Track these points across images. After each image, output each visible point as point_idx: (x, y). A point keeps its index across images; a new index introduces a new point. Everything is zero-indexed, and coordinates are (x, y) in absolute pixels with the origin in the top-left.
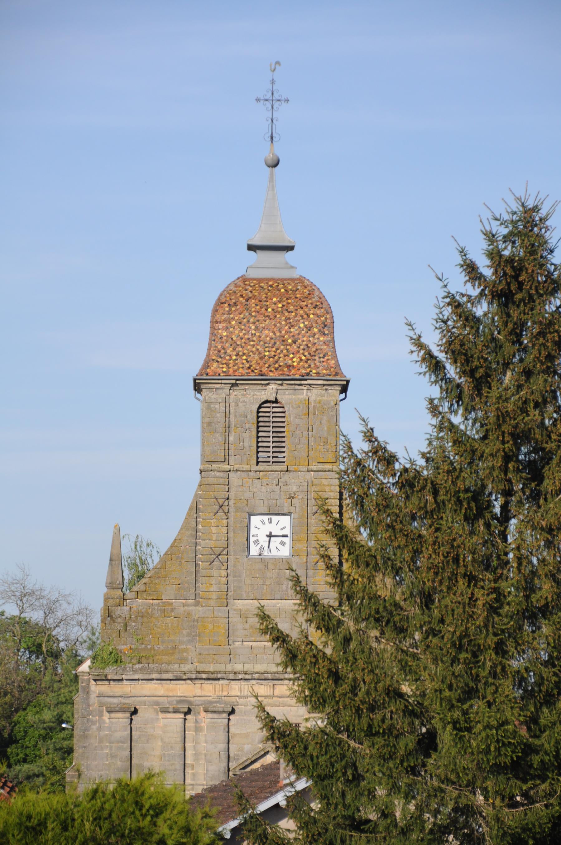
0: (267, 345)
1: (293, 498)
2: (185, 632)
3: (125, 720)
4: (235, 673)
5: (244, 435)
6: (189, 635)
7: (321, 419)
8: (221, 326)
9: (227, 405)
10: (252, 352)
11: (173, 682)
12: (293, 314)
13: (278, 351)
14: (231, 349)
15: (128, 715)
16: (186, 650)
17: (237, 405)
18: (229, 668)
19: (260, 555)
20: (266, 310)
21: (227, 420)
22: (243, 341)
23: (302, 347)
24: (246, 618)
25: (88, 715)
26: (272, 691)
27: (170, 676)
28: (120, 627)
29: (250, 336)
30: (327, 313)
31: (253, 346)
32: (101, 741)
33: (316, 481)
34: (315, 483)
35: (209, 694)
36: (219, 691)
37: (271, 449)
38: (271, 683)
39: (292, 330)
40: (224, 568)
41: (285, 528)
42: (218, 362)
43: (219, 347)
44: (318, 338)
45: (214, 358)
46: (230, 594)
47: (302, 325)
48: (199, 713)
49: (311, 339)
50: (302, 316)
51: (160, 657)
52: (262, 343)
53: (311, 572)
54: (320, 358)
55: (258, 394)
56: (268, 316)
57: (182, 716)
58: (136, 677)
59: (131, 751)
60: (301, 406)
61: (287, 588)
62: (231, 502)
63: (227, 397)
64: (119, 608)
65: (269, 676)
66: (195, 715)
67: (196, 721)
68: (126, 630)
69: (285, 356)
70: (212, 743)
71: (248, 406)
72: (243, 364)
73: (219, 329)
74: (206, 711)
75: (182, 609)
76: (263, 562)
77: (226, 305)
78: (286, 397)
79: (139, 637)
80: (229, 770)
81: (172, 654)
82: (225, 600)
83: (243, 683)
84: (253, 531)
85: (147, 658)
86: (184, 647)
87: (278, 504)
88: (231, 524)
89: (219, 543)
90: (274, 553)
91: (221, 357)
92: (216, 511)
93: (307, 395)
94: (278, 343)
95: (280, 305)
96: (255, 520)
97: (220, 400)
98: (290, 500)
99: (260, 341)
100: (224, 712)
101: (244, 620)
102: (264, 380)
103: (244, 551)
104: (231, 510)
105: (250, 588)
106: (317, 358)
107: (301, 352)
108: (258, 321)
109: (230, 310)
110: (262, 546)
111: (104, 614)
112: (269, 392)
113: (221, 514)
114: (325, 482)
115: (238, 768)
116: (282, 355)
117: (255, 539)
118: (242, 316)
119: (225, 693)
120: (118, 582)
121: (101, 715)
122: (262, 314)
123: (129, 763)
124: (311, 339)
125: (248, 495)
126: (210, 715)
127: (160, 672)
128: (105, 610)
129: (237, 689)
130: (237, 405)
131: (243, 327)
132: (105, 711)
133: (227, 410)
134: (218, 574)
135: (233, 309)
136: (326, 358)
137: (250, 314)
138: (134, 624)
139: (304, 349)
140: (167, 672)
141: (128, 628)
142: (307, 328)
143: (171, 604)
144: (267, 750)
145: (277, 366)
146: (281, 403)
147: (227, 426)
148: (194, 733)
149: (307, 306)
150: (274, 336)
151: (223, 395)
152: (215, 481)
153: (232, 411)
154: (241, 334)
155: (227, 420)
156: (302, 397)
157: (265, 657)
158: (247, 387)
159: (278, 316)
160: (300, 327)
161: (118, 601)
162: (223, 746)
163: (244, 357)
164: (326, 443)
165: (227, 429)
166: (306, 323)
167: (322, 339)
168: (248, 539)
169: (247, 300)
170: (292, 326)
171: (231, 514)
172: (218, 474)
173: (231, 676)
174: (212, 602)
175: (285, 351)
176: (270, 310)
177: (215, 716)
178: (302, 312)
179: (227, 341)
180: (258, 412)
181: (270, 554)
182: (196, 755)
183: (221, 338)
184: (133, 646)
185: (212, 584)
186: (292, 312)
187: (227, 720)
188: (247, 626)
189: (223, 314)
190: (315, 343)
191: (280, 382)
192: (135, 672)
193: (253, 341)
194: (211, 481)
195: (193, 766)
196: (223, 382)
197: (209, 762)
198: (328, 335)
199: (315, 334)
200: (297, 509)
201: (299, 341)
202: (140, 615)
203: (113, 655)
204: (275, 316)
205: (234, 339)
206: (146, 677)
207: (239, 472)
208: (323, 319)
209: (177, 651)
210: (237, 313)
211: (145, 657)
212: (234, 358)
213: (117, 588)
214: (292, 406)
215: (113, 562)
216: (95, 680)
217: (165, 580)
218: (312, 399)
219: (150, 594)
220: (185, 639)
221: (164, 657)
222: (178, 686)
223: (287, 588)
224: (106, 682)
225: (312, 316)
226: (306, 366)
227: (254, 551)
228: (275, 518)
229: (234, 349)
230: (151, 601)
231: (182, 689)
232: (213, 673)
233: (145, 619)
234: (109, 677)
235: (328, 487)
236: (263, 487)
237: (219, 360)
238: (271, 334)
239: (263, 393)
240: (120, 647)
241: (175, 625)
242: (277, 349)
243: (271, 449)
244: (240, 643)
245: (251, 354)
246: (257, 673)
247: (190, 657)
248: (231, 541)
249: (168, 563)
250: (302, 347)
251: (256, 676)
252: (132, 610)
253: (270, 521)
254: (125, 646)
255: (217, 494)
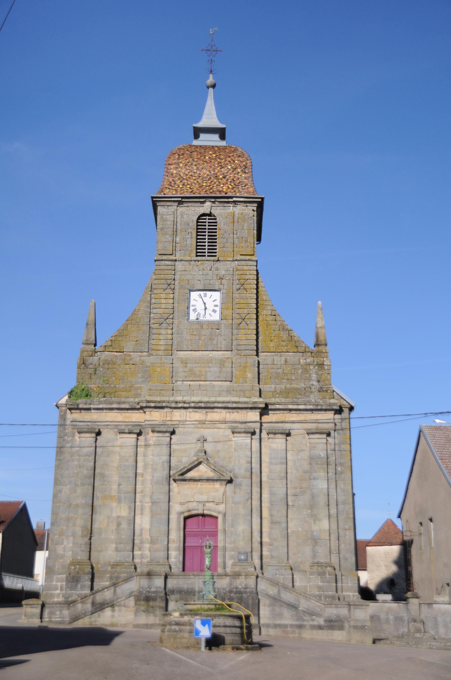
0: (204, 179)
1: (222, 279)
2: (140, 375)
3: (91, 439)
4: (176, 402)
5: (187, 236)
6: (142, 377)
7: (243, 225)
8: (172, 167)
9: (175, 216)
10: (194, 183)
11: (129, 411)
12: (224, 160)
13: (213, 183)
14: (179, 181)
15: (94, 435)
16: (140, 388)
17: (182, 217)
18: (172, 399)
19: (197, 319)
20: (205, 158)
21: (175, 226)
22: (188, 176)
23: (229, 181)
24: (186, 363)
25: (64, 436)
26: (205, 417)
27: (127, 406)
28: (91, 371)
29: (193, 174)
30: (247, 160)
31: (195, 179)
32: (72, 455)
33: (239, 268)
34: (238, 269)
35: (156, 419)
36: (164, 417)
37: (207, 221)
38: (204, 411)
39: (222, 170)
40: (170, 328)
41: (216, 300)
42: (169, 189)
43: (171, 180)
44: (241, 175)
45: (167, 186)
46: (174, 347)
47: (230, 167)
48: (148, 433)
49: (236, 176)
50: (230, 162)
51: (120, 393)
52: (201, 178)
53: (235, 332)
54: (242, 187)
55: (198, 209)
56: (206, 162)
57: (135, 436)
58: (101, 406)
59: (95, 462)
60: (228, 217)
61: (217, 342)
62: (176, 283)
63: (175, 212)
64: (91, 357)
65: (203, 405)
66: (145, 436)
67: (146, 440)
68: (95, 373)
69: (217, 185)
70: (157, 456)
71: (190, 217)
72: (187, 190)
73: (171, 169)
74: (153, 431)
75: (138, 358)
76: (199, 323)
77: (177, 155)
78: (218, 211)
79: (105, 379)
80: (170, 477)
81: (130, 391)
82: (170, 350)
83: (183, 411)
84: (192, 302)
85: (110, 394)
86: (139, 385)
87: (211, 283)
88: (176, 297)
89: (167, 311)
90: (208, 318)
91: (171, 186)
92: (165, 288)
93: (233, 210)
94: (212, 178)
95: (214, 155)
96: (194, 295)
97: (170, 213)
98: (220, 280)
99: (199, 177)
100: (166, 432)
101: (185, 365)
102: (202, 199)
103: (185, 316)
104: (176, 288)
105: (189, 342)
106: (240, 187)
107: (229, 183)
108: (199, 164)
109: (179, 158)
110: (199, 313)
111: (80, 362)
112: (207, 207)
113: (169, 291)
114: (245, 268)
115: (177, 474)
116: (215, 185)
117: (194, 308)
118: (187, 161)
119: (168, 419)
120: (91, 340)
121: (73, 436)
122: (201, 160)
123: (93, 471)
124: (236, 176)
125: (188, 277)
126: (156, 434)
127: (119, 403)
128: (80, 359)
129: (178, 415)
130: (182, 217)
131: (188, 168)
132: (77, 432)
133: (175, 220)
134: (165, 332)
135: (181, 157)
136: (247, 187)
137: (193, 160)
138: (102, 369)
139: (231, 182)
140: (124, 403)
141: (97, 372)
142: (233, 169)
143: (130, 356)
144: (200, 460)
145: (211, 191)
146: (214, 216)
147: (175, 230)
148: (144, 449)
149: (233, 156)
150: (209, 174)
151: (173, 210)
152: (165, 267)
153: (179, 220)
154: (186, 172)
155: (175, 226)
156: (229, 211)
157: (200, 392)
158: (190, 204)
159: (213, 161)
160: (228, 168)
161: (91, 353)
162: (166, 458)
163: (188, 186)
164: (246, 241)
165: (175, 233)
166: (233, 166)
167: (243, 175)
168: (188, 308)
169: (191, 152)
170: (223, 167)
171: (176, 291)
172: (167, 263)
173: (173, 405)
174: (160, 353)
175: (217, 183)
176: (207, 158)
177: (160, 435)
178: (229, 159)
179: (176, 176)
180: (198, 222)
181: (205, 319)
182: (145, 466)
183: (172, 174)
184: (100, 385)
185: (162, 338)
186: (222, 159)
187: (169, 438)
188: (187, 369)
189: (174, 160)
190: (239, 178)
191: (213, 200)
192: (100, 403)
193: (195, 177)
194: (162, 267)
195: (142, 475)
196: (172, 199)
197: (154, 470)
198: (248, 173)
199: (238, 173)
200: (225, 287)
201: (228, 177)
202: (107, 362)
203: (84, 391)
204: (211, 162)
205: (182, 175)
206: (109, 406)
207: (182, 262)
208: (244, 163)
209: (133, 388)
210: (184, 159)
211: (109, 393)
212: (181, 186)
213: (90, 344)
214: (222, 217)
215: (89, 326)
216: (70, 409)
217: (126, 338)
218: (236, 213)
219: (115, 348)
220: (140, 380)
221: (123, 393)
222: (134, 414)
223: (217, 342)
224: (78, 411)
225: (236, 162)
226: (233, 191)
227: (193, 316)
228: (209, 293)
229: (181, 181)
230: (116, 353)
231: (136, 417)
232: (159, 402)
233: (110, 366)
234: (81, 406)
235: (248, 271)
236: (200, 271)
237: (171, 188)
238: (208, 172)
239: (201, 208)
240: (90, 386)
241: (133, 370)
242: (211, 182)
243: (207, 221)
244: (181, 382)
245: (193, 184)
246: (193, 402)
247: (143, 393)
248: (176, 309)
249: (129, 326)
250: (229, 181)
251: (192, 405)
252: (101, 359)
253: (205, 296)
254: (95, 385)
255: (166, 277)
